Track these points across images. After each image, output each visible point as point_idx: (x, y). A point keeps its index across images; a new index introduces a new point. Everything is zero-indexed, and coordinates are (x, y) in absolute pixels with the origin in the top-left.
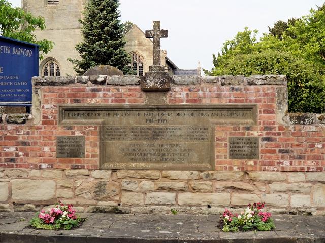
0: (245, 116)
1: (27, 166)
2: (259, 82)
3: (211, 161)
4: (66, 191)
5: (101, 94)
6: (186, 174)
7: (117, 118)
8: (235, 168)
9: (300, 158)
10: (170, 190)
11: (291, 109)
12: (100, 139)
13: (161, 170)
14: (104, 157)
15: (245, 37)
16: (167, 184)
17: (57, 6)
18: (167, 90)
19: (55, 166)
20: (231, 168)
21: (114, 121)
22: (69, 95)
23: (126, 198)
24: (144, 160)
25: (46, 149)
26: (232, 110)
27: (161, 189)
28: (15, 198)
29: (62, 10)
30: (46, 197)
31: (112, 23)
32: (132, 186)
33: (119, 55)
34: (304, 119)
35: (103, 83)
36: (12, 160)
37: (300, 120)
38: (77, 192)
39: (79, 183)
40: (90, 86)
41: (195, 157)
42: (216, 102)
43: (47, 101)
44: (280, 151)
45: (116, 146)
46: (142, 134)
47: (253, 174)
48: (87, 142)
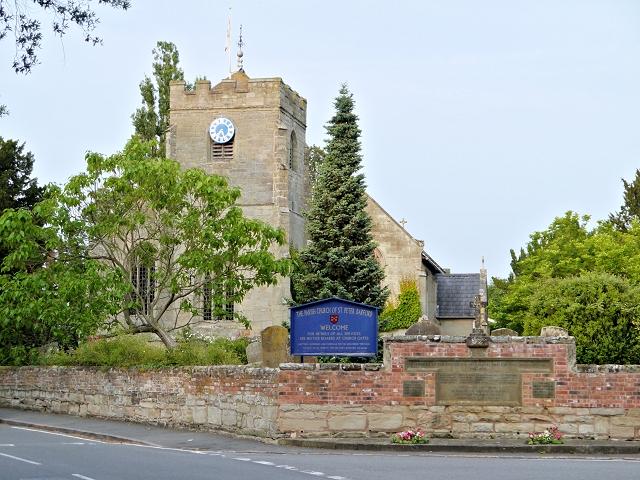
0: (544, 366)
1: (381, 403)
2: (554, 342)
3: (520, 399)
4: (410, 421)
5: (437, 349)
6: (500, 409)
7: (449, 367)
8: (538, 405)
9: (585, 397)
10: (489, 421)
11: (578, 362)
12: (436, 383)
13: (482, 406)
14: (439, 396)
15: (569, 227)
16: (486, 416)
17: (230, 165)
18: (486, 347)
19: (403, 402)
20: (534, 405)
21: (447, 369)
22: (412, 350)
23: (456, 427)
24: (470, 399)
25: (395, 390)
26: (535, 362)
27: (482, 420)
28: (371, 427)
29: (238, 170)
30: (395, 427)
31: (356, 218)
32: (460, 418)
33: (367, 269)
34: (587, 369)
35: (438, 341)
36: (368, 398)
37: (585, 370)
38: (419, 423)
39: (420, 416)
40: (429, 344)
41: (507, 396)
42: (523, 356)
43: (395, 354)
44: (571, 392)
45: (447, 388)
46: (469, 379)
47: (550, 409)
48: (427, 385)
